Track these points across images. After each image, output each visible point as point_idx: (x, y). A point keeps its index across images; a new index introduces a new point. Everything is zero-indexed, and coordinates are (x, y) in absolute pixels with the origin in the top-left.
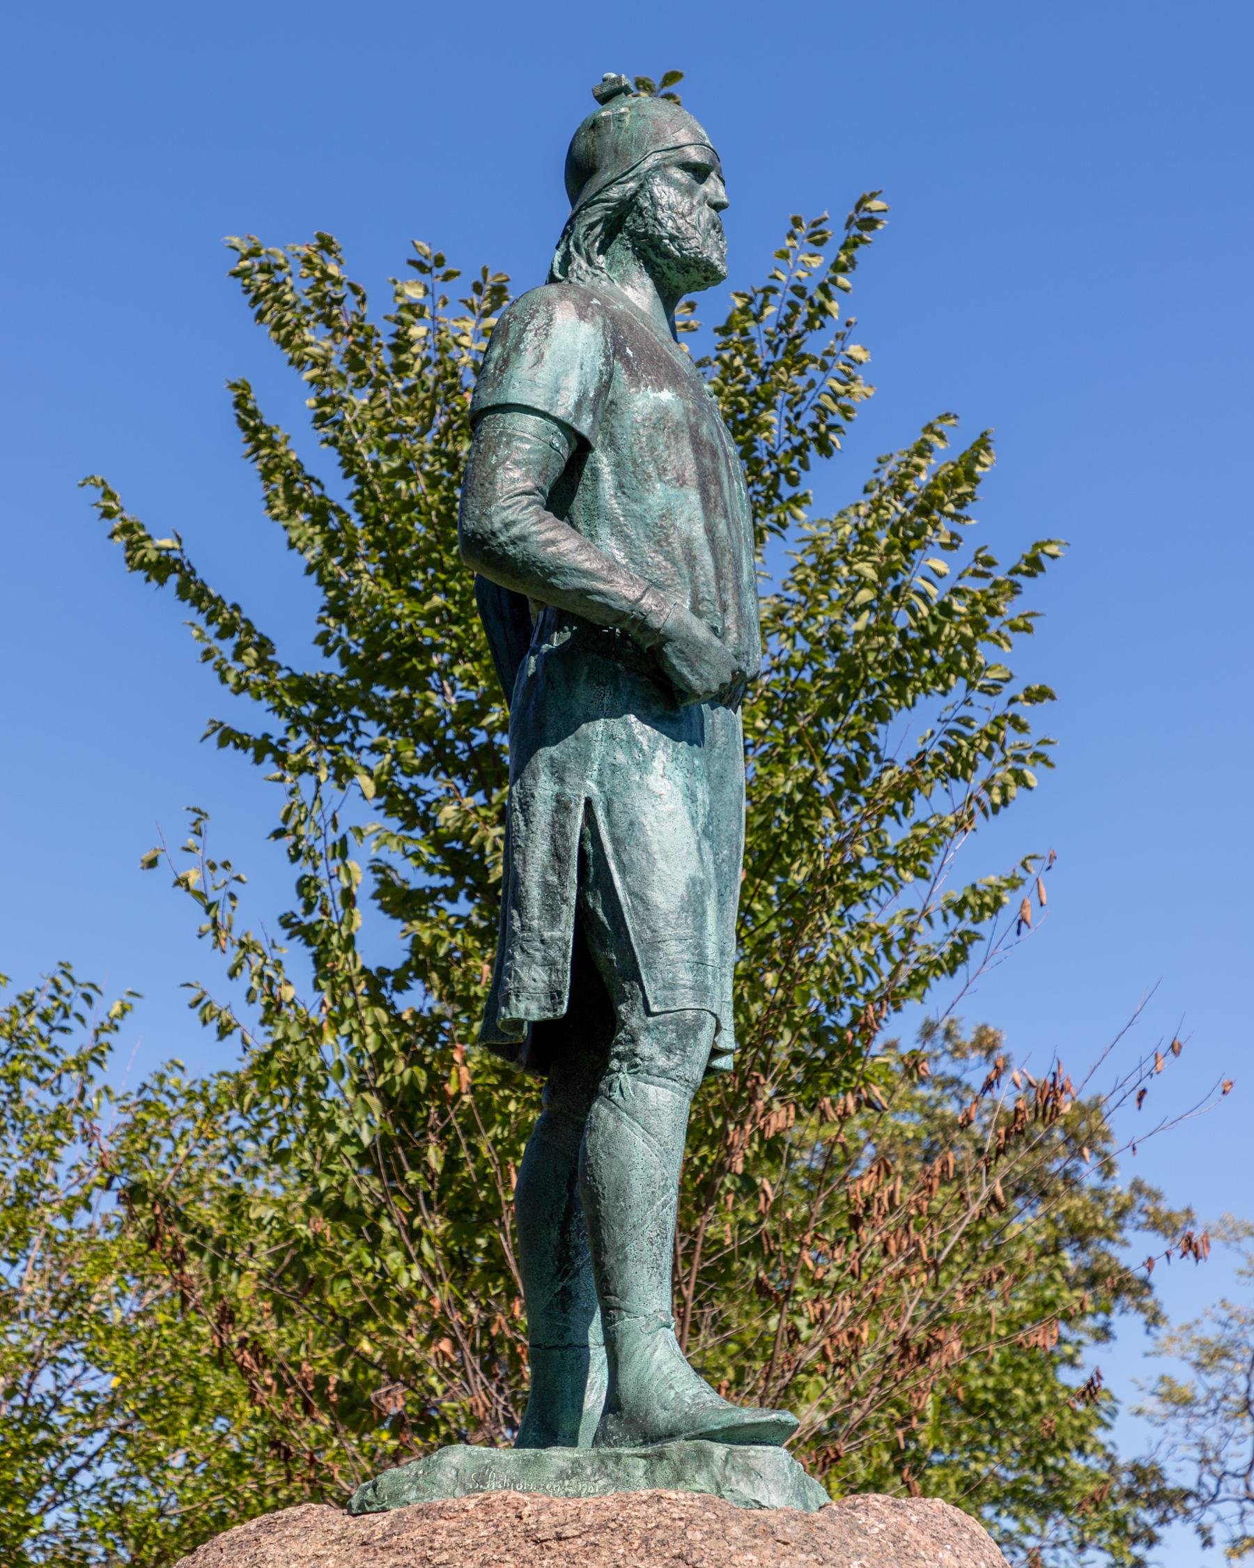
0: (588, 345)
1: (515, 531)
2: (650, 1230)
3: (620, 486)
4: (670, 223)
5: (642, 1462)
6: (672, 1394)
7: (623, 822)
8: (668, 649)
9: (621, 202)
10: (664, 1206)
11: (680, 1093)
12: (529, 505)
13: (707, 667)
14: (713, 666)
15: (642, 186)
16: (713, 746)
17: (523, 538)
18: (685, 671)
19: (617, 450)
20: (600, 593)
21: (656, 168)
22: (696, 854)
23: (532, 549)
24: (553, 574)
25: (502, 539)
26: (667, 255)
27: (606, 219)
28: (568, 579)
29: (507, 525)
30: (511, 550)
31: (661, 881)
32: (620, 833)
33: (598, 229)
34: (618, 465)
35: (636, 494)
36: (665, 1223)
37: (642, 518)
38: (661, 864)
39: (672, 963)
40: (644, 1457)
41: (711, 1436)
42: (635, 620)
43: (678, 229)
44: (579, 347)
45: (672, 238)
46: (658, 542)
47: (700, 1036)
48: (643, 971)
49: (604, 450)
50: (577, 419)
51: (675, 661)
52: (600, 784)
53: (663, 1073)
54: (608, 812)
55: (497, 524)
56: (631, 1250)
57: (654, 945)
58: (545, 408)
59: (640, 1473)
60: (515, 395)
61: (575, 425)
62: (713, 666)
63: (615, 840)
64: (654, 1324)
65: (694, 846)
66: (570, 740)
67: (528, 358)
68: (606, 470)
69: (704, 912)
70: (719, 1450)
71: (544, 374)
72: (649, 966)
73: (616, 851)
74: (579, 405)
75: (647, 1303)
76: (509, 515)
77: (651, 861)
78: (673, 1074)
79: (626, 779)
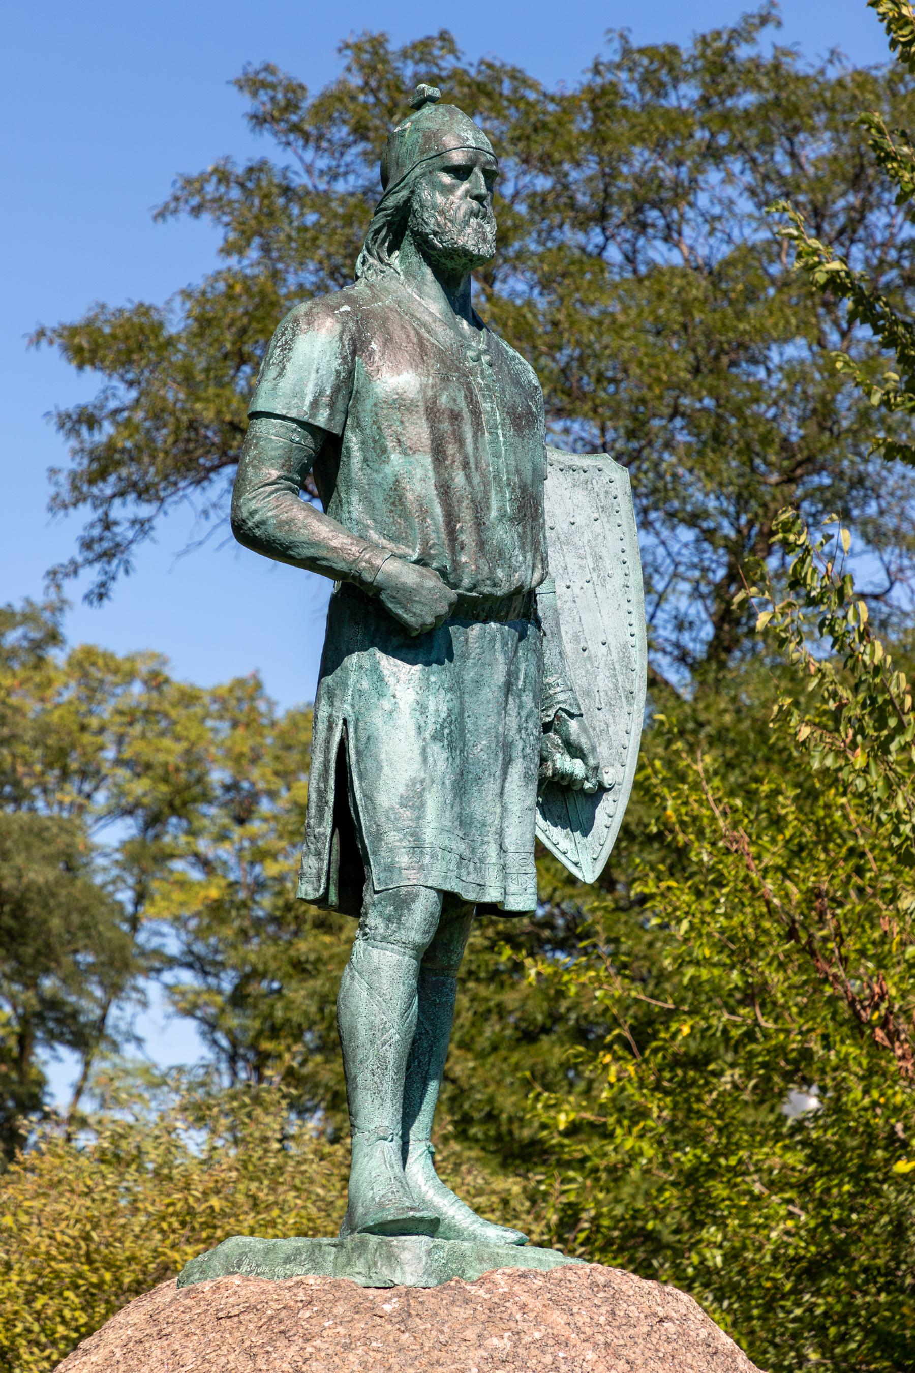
0: (324, 352)
1: (257, 517)
2: (372, 1063)
3: (365, 460)
4: (432, 221)
5: (334, 1250)
6: (370, 1194)
7: (363, 736)
8: (383, 597)
9: (397, 208)
10: (384, 1044)
11: (399, 953)
12: (272, 493)
13: (419, 606)
14: (424, 604)
15: (412, 192)
16: (465, 657)
17: (263, 522)
18: (400, 612)
19: (362, 431)
20: (324, 559)
21: (423, 175)
22: (419, 759)
23: (271, 530)
24: (288, 548)
25: (250, 524)
26: (434, 247)
27: (389, 224)
28: (300, 551)
29: (252, 513)
30: (258, 533)
31: (386, 784)
32: (362, 746)
33: (383, 233)
34: (363, 443)
35: (376, 466)
36: (385, 1057)
37: (381, 484)
38: (386, 770)
39: (391, 850)
40: (335, 1246)
41: (370, 1230)
42: (354, 577)
43: (439, 225)
44: (316, 355)
45: (435, 234)
46: (393, 504)
47: (413, 906)
48: (371, 858)
49: (354, 432)
50: (313, 415)
51: (390, 605)
52: (353, 706)
53: (384, 939)
54: (356, 729)
55: (245, 514)
56: (360, 1080)
57: (378, 836)
58: (284, 412)
59: (332, 1258)
60: (261, 405)
61: (311, 421)
62: (424, 604)
63: (358, 753)
64: (374, 1138)
65: (417, 751)
66: (338, 671)
67: (272, 373)
68: (356, 448)
69: (423, 805)
70: (374, 1239)
71: (286, 385)
72: (375, 853)
73: (358, 762)
74: (315, 404)
75: (370, 1121)
76: (253, 505)
77: (380, 768)
78: (392, 939)
79: (367, 701)
